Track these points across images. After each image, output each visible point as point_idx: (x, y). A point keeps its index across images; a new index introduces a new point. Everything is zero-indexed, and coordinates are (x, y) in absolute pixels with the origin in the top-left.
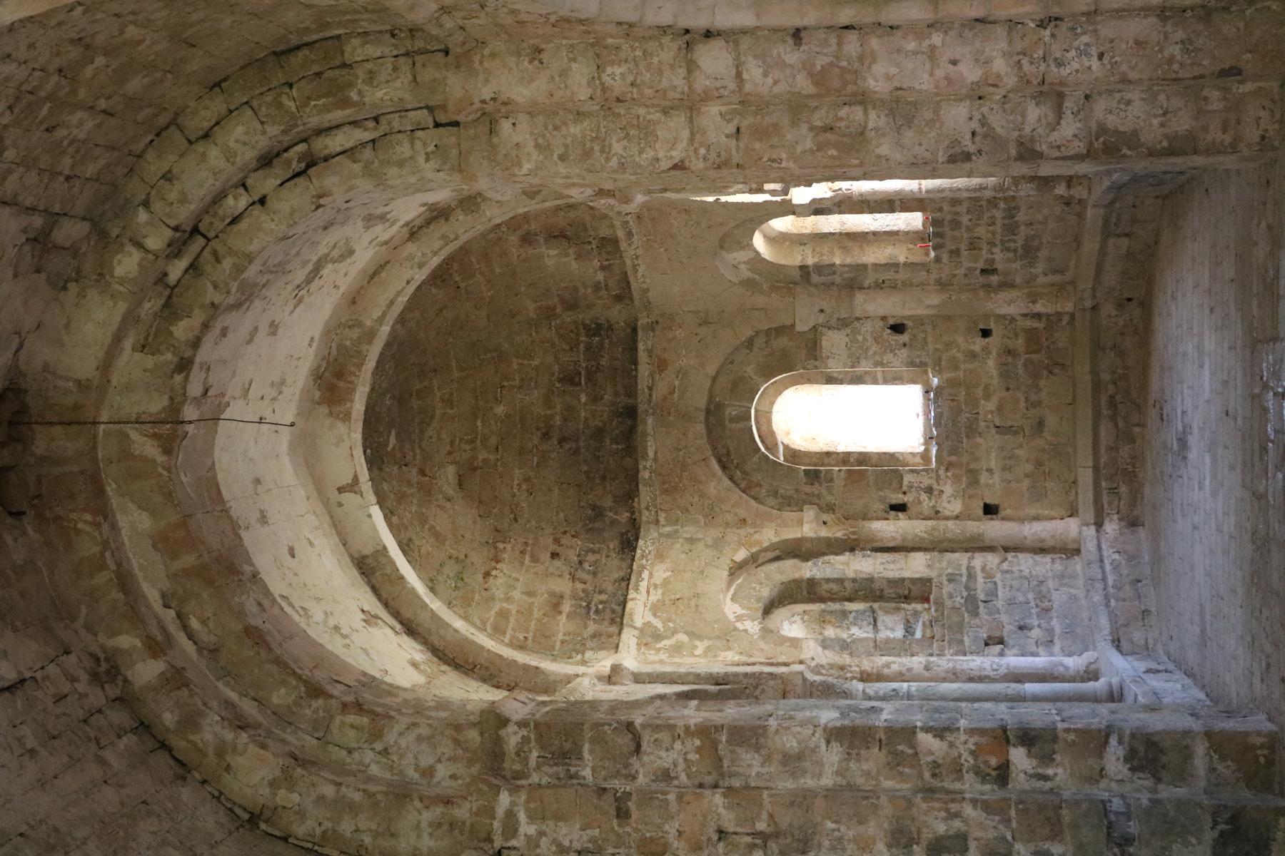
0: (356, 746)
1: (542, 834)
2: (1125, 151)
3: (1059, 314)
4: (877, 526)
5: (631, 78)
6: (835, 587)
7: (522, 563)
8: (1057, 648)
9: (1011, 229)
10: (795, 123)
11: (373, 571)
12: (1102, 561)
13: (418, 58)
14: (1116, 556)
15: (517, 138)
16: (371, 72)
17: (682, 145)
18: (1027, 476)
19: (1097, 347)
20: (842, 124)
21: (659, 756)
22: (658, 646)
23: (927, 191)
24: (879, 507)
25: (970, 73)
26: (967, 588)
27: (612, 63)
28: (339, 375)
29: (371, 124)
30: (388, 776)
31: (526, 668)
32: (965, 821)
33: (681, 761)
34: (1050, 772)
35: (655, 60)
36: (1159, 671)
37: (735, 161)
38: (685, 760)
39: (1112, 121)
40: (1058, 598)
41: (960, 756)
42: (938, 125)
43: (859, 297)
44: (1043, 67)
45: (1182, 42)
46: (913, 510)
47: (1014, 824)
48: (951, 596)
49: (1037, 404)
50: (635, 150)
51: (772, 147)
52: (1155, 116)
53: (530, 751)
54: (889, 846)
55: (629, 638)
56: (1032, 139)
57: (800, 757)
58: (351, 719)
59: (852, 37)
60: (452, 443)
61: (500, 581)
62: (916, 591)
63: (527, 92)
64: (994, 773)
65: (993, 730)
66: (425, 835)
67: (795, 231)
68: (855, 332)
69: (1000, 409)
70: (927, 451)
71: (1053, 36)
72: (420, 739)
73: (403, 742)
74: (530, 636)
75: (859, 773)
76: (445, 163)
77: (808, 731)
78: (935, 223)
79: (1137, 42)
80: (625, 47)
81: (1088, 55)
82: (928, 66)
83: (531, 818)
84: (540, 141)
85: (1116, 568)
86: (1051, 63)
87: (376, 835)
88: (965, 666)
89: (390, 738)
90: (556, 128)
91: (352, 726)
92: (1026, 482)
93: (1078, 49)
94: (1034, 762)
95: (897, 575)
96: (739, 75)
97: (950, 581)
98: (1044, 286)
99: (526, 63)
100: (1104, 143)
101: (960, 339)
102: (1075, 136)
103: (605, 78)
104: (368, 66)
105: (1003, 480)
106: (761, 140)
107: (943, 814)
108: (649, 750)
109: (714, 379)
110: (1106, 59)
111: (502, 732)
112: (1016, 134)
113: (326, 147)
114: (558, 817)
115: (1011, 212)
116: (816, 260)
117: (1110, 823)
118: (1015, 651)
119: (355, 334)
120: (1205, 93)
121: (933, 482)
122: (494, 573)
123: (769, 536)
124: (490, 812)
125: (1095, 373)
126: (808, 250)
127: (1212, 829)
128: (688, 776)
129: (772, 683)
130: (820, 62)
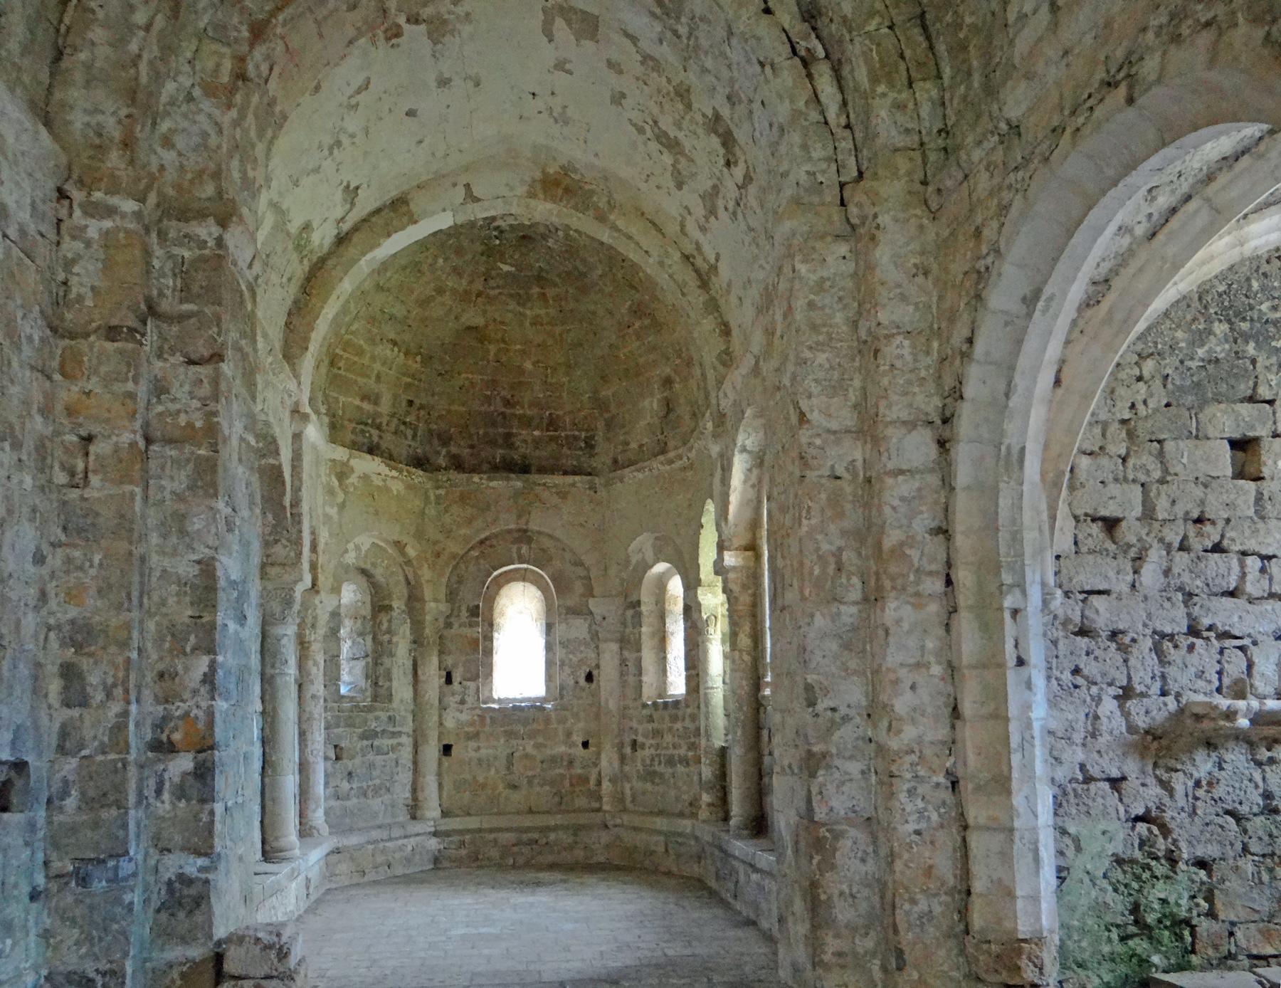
0: (197, 68)
1: (88, 244)
2: (817, 859)
3: (599, 798)
4: (435, 660)
5: (898, 364)
6: (385, 626)
7: (404, 375)
8: (333, 803)
9: (671, 762)
10: (844, 533)
11: (395, 211)
12: (406, 837)
13: (917, 155)
14: (410, 848)
15: (830, 259)
16: (905, 106)
17: (826, 423)
18: (474, 777)
19: (577, 829)
20: (844, 580)
21: (183, 383)
22: (334, 479)
23: (706, 694)
24: (449, 661)
25: (902, 704)
26: (384, 731)
27: (913, 346)
28: (567, 190)
29: (843, 121)
30: (164, 98)
31: (306, 339)
32: (102, 705)
33: (178, 406)
34: (166, 796)
35: (916, 390)
36: (308, 888)
37: (808, 473)
38: (179, 411)
39: (845, 844)
40: (376, 804)
41: (182, 701)
42: (843, 674)
43: (614, 647)
44: (908, 776)
45: (931, 912)
46: (447, 689)
47: (100, 758)
48: (377, 718)
49: (530, 783)
50: (821, 375)
51: (823, 510)
52: (850, 887)
53: (190, 249)
54: (72, 622)
55: (340, 453)
56: (829, 767)
57: (183, 532)
58: (227, 65)
59: (938, 585)
60: (502, 323)
61: (388, 352)
62: (382, 692)
63: (885, 259)
64: (164, 738)
65: (212, 735)
66: (87, 119)
67: (667, 596)
68: (587, 644)
69: (527, 756)
70: (494, 701)
71: (938, 785)
72: (205, 135)
73: (201, 118)
74: (342, 372)
75: (164, 594)
76: (806, 190)
77: (211, 541)
78: (676, 703)
79: (931, 867)
80: (929, 360)
81: (918, 821)
82: (912, 661)
83: (106, 234)
84: (828, 283)
85: (401, 849)
86: (913, 784)
87: (88, 67)
88: (315, 727)
89: (206, 105)
90: (840, 299)
91: (218, 65)
92: (468, 777)
93: (926, 810)
94: (177, 780)
95: (395, 676)
96: (902, 472)
97: (390, 718)
98: (623, 787)
99: (913, 261)
100: (825, 837)
101: (581, 725)
102: (831, 810)
103: (899, 338)
104: (911, 105)
105: (470, 759)
106: (829, 499)
107: (110, 681)
108: (190, 373)
109: (551, 536)
110: (915, 838)
111: (211, 220)
112: (834, 751)
113: (821, 75)
114: (108, 266)
115: (685, 761)
116: (645, 613)
117: (104, 861)
118: (330, 770)
119: (602, 204)
120: (872, 933)
121: (469, 705)
122: (396, 349)
123: (426, 573)
124: (114, 188)
125: (555, 829)
126: (652, 607)
127: (97, 971)
128: (160, 414)
129: (292, 554)
130: (914, 554)
